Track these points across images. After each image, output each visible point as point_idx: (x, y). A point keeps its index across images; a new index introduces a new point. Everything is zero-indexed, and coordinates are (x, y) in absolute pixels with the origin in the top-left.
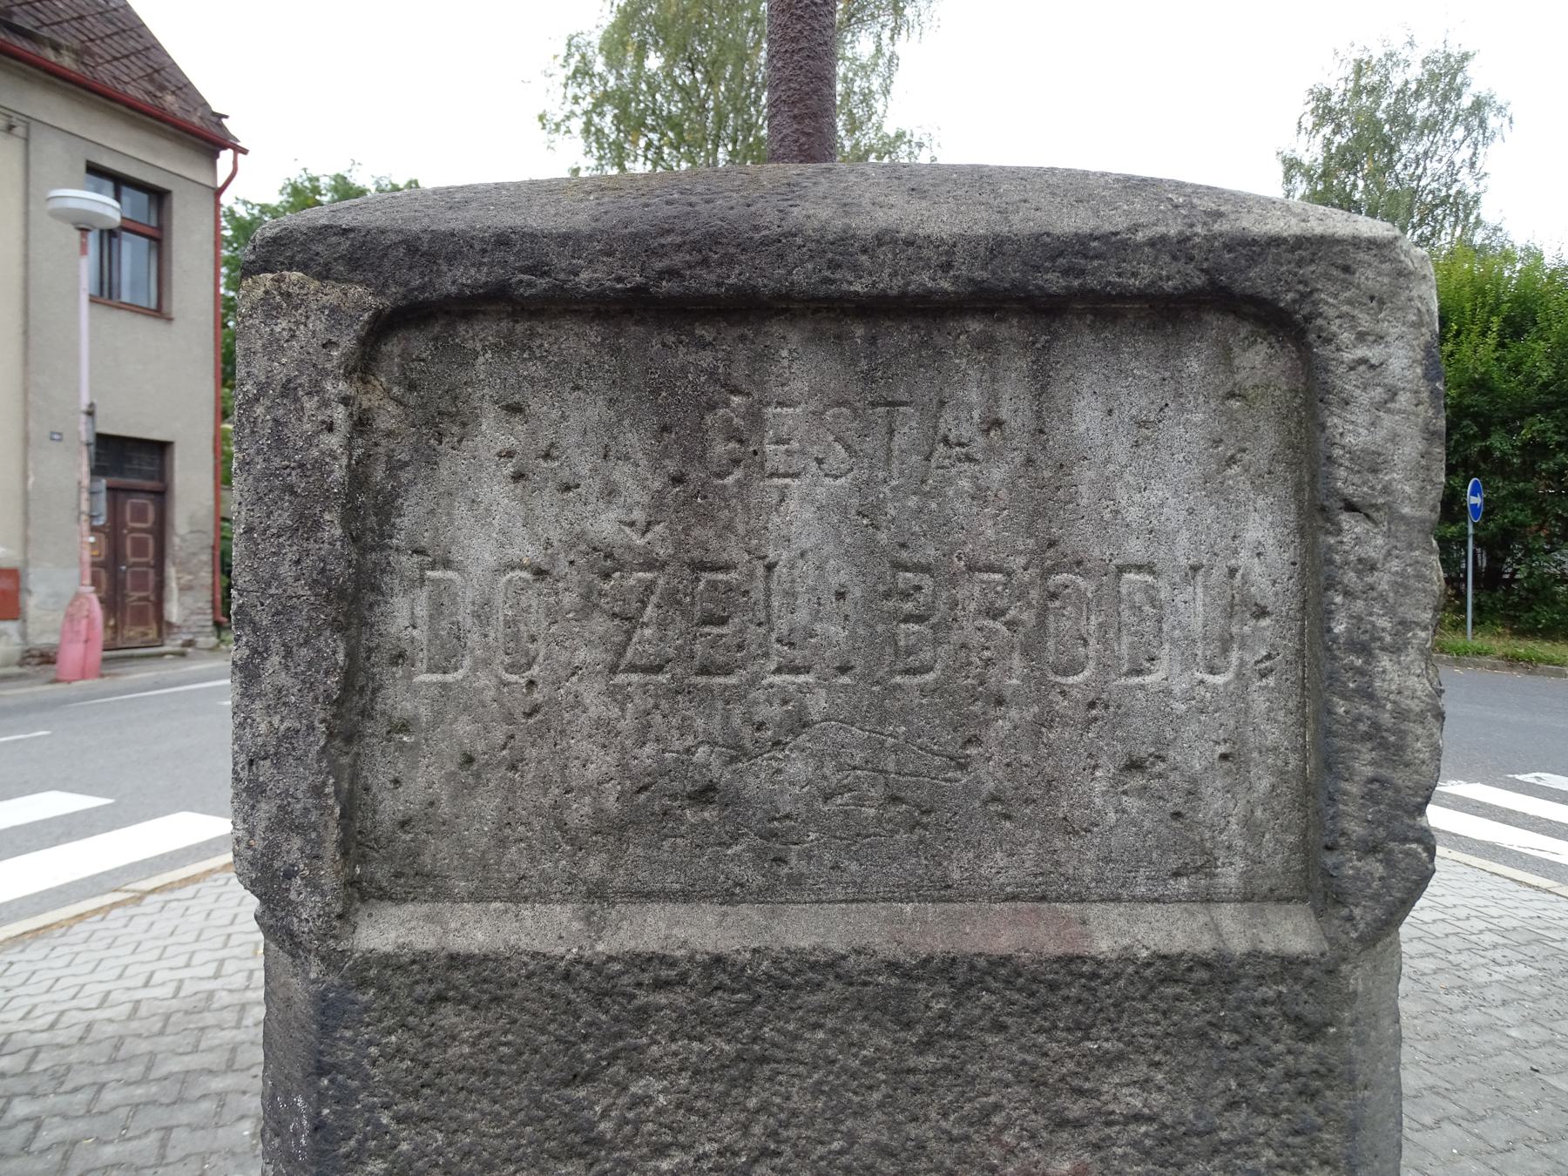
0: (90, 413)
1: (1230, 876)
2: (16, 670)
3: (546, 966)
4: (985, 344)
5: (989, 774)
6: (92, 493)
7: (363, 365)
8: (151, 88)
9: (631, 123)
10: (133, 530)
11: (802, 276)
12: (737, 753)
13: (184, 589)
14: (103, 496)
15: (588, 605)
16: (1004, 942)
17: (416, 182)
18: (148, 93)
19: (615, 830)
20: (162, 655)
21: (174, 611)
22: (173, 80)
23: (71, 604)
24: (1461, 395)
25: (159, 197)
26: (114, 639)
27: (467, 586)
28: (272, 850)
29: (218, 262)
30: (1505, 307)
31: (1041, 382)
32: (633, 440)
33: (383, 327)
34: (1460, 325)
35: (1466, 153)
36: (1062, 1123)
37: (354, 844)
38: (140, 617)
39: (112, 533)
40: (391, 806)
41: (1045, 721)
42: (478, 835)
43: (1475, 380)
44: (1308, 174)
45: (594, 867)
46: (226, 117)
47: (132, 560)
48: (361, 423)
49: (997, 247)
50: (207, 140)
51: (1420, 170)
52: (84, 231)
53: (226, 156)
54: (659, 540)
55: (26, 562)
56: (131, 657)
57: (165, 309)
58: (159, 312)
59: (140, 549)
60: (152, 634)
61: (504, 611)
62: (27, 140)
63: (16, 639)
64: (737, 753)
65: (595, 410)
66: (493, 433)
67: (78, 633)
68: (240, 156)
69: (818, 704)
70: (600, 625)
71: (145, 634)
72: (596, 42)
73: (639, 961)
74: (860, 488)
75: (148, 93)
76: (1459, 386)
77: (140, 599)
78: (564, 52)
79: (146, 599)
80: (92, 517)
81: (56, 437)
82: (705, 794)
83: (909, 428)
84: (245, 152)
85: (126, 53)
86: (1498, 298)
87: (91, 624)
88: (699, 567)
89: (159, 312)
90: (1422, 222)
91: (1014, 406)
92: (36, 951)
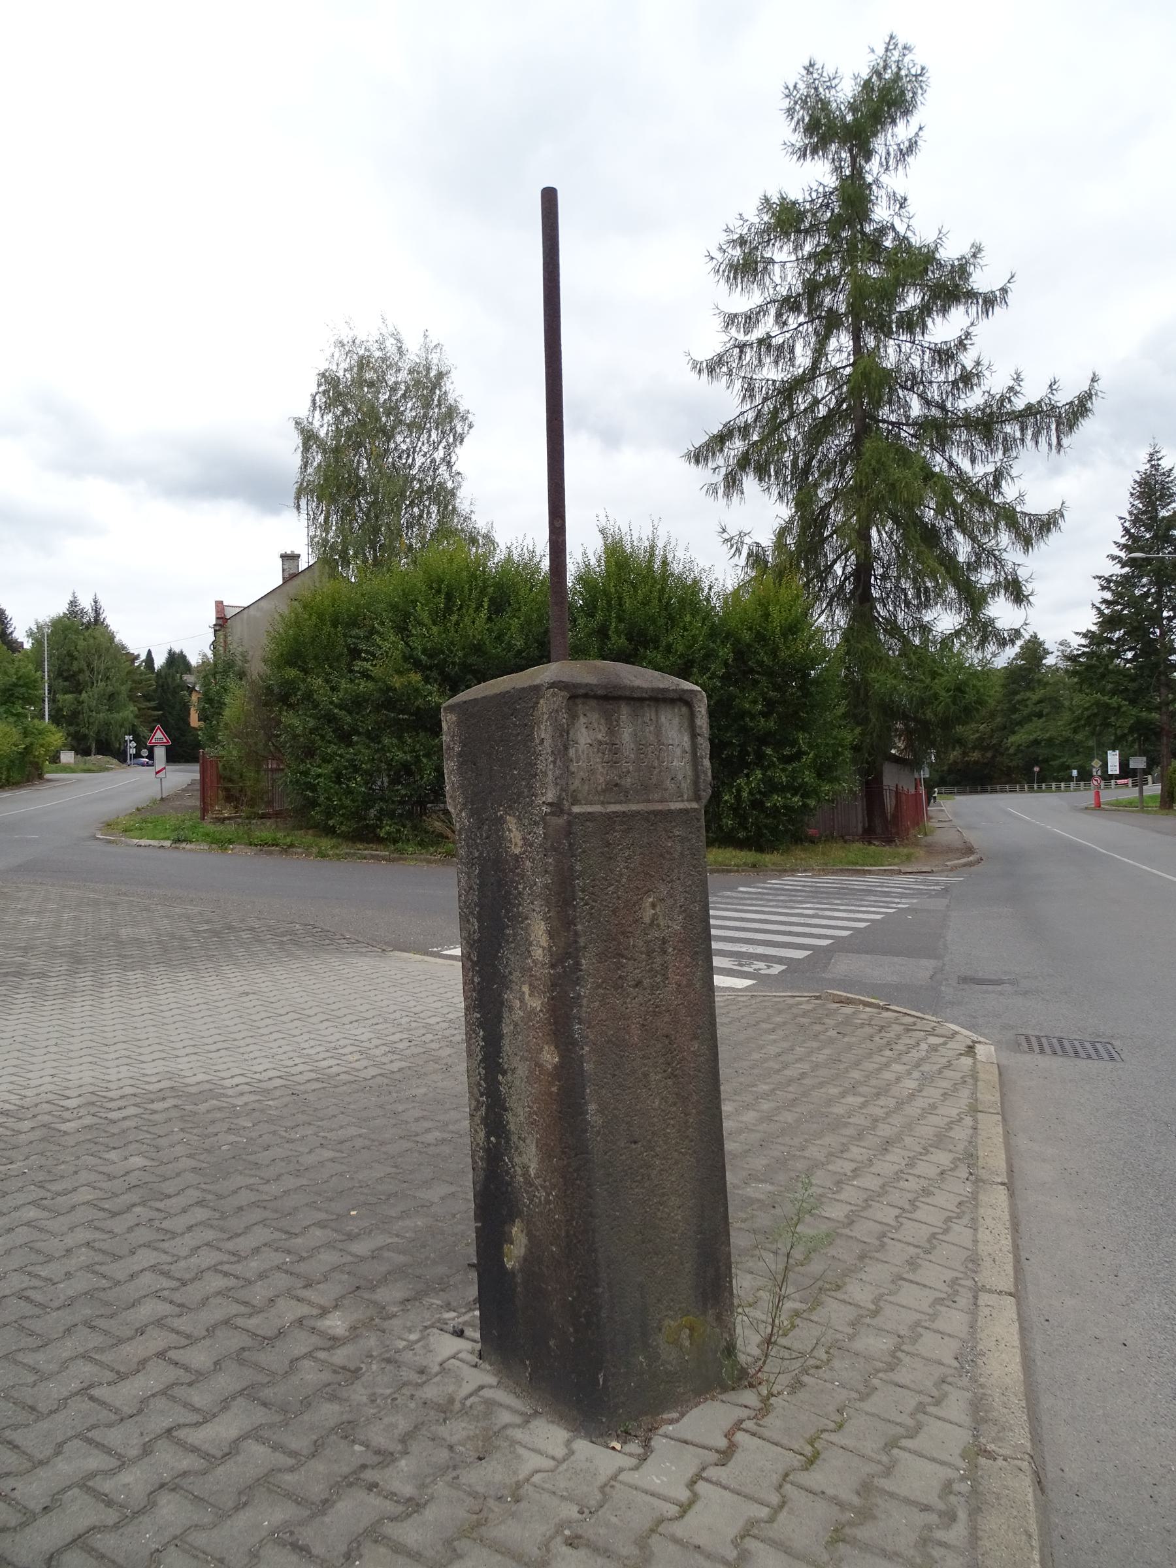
1: (685, 797)
4: (649, 705)
5: (654, 781)
11: (628, 693)
12: (620, 778)
15: (598, 751)
16: (660, 808)
19: (604, 791)
24: (465, 656)
28: (560, 795)
30: (491, 590)
31: (657, 711)
32: (603, 721)
34: (463, 601)
35: (439, 454)
36: (669, 837)
41: (660, 772)
43: (474, 645)
44: (322, 445)
45: (602, 799)
49: (653, 689)
51: (410, 461)
61: (586, 752)
64: (620, 778)
65: (597, 716)
66: (582, 720)
69: (631, 769)
70: (600, 755)
73: (614, 812)
74: (634, 730)
76: (464, 649)
82: (616, 785)
83: (640, 721)
86: (484, 582)
88: (613, 744)
90: (412, 504)
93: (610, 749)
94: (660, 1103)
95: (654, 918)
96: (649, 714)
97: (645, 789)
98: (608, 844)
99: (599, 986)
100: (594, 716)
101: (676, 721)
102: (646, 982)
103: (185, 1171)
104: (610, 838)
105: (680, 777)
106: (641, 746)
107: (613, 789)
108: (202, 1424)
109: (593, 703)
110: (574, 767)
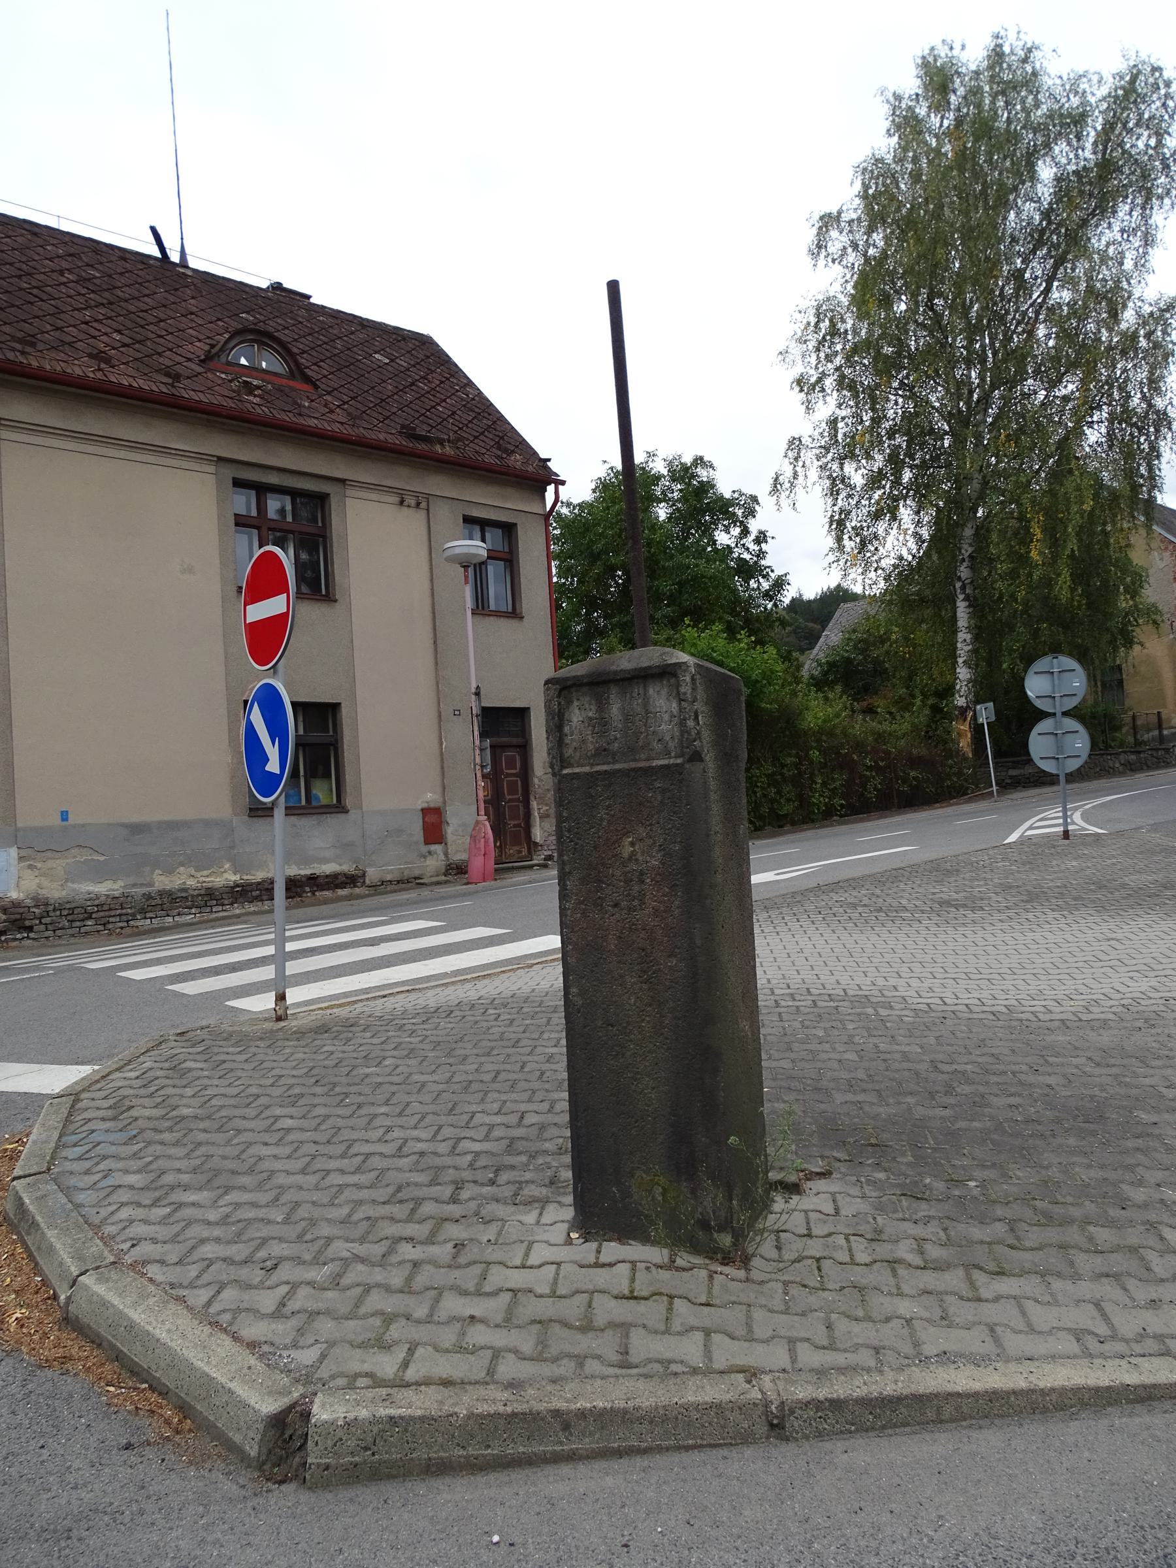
0: (477, 694)
2: (443, 878)
3: (587, 774)
5: (640, 744)
6: (481, 750)
7: (559, 696)
8: (499, 453)
9: (885, 367)
10: (508, 775)
13: (543, 817)
14: (488, 751)
17: (701, 458)
18: (498, 457)
19: (593, 756)
20: (531, 867)
21: (538, 834)
22: (511, 441)
23: (474, 829)
25: (509, 529)
26: (501, 856)
27: (574, 724)
29: (550, 556)
33: (561, 690)
37: (562, 761)
38: (516, 840)
39: (494, 778)
40: (566, 755)
42: (577, 758)
46: (549, 460)
47: (508, 797)
48: (559, 704)
50: (536, 480)
52: (466, 567)
53: (551, 489)
54: (597, 716)
55: (444, 803)
56: (513, 868)
57: (518, 611)
58: (515, 614)
59: (513, 791)
60: (525, 852)
62: (428, 510)
63: (442, 857)
66: (576, 703)
67: (479, 849)
68: (560, 487)
71: (520, 852)
72: (845, 301)
75: (498, 457)
77: (515, 826)
78: (813, 320)
79: (519, 826)
80: (482, 767)
81: (457, 713)
82: (605, 750)
84: (563, 483)
85: (481, 430)
87: (486, 842)
89: (515, 614)
91: (641, 691)
92: (486, 981)
93: (601, 724)
94: (635, 1002)
95: (633, 854)
96: (637, 690)
97: (631, 751)
98: (591, 796)
99: (581, 903)
100: (586, 700)
101: (664, 692)
102: (624, 904)
103: (1050, 1245)
104: (592, 792)
105: (667, 738)
106: (628, 717)
107: (602, 753)
108: (824, 1348)
109: (585, 689)
110: (568, 740)
